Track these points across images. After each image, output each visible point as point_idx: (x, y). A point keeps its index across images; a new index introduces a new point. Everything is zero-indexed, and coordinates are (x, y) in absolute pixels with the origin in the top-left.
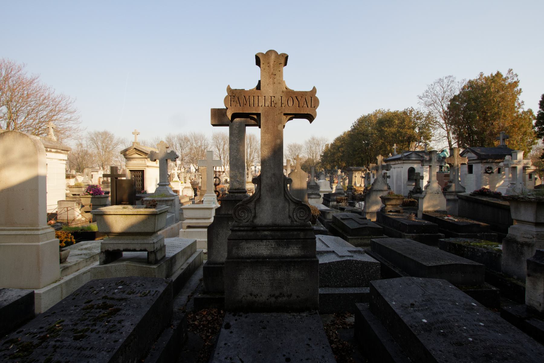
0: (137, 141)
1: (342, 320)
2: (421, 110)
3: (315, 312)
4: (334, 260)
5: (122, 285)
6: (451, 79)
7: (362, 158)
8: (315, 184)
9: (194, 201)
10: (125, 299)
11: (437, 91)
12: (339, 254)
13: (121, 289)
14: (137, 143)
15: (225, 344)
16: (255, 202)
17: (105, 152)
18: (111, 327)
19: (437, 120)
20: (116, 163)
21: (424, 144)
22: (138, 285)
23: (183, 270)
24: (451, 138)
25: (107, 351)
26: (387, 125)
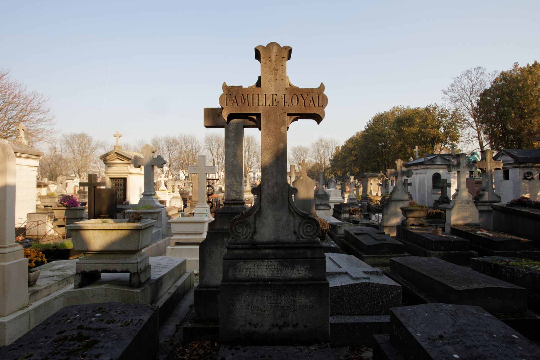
0: (119, 144)
1: (357, 355)
2: (447, 106)
3: (325, 345)
4: (348, 283)
5: (101, 313)
6: (481, 71)
7: (379, 163)
8: (324, 193)
9: (184, 213)
10: (103, 329)
12: (353, 276)
13: (99, 317)
14: (119, 147)
17: (82, 157)
19: (465, 117)
22: (119, 312)
24: (483, 139)
26: (407, 124)
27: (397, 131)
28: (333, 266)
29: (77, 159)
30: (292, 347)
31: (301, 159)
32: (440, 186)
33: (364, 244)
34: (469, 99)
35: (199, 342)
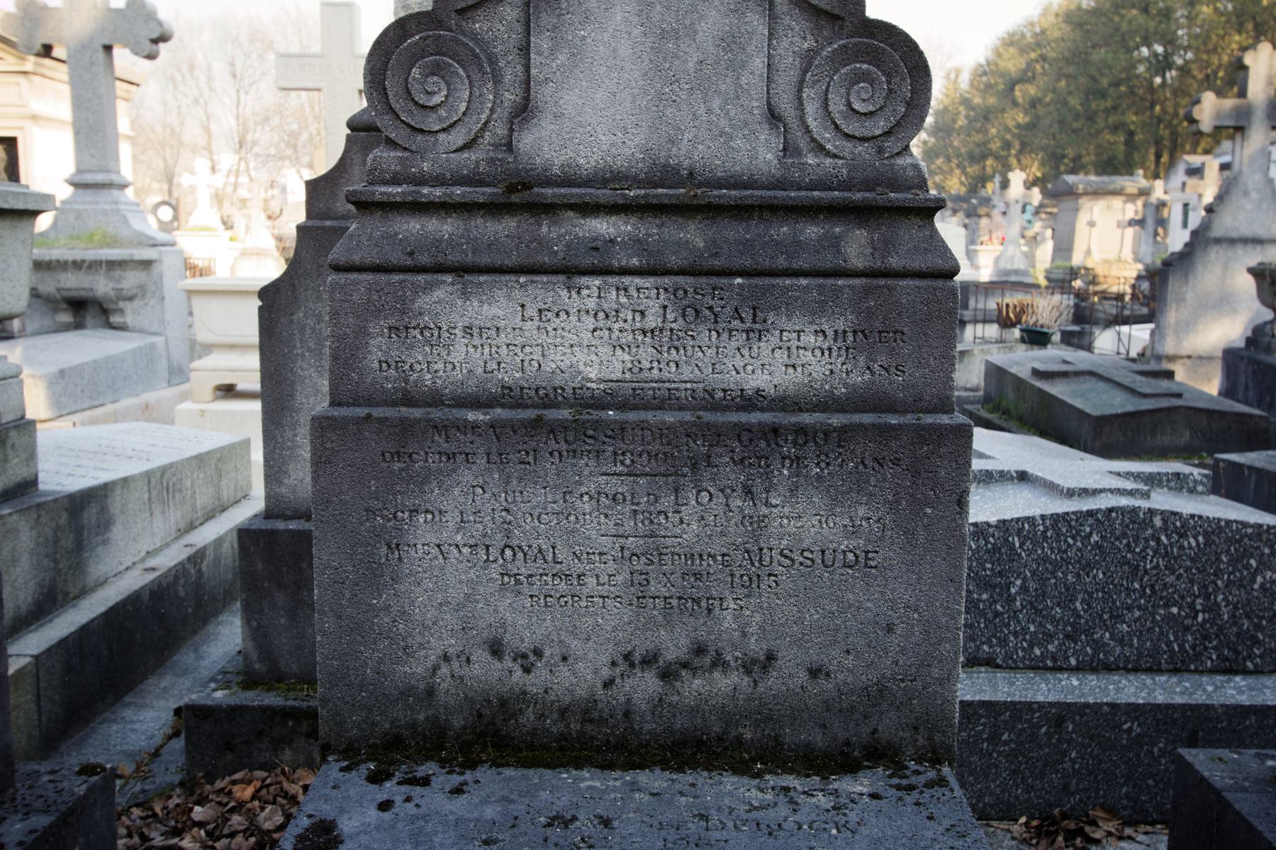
3: (932, 774)
30: (735, 779)
35: (266, 774)
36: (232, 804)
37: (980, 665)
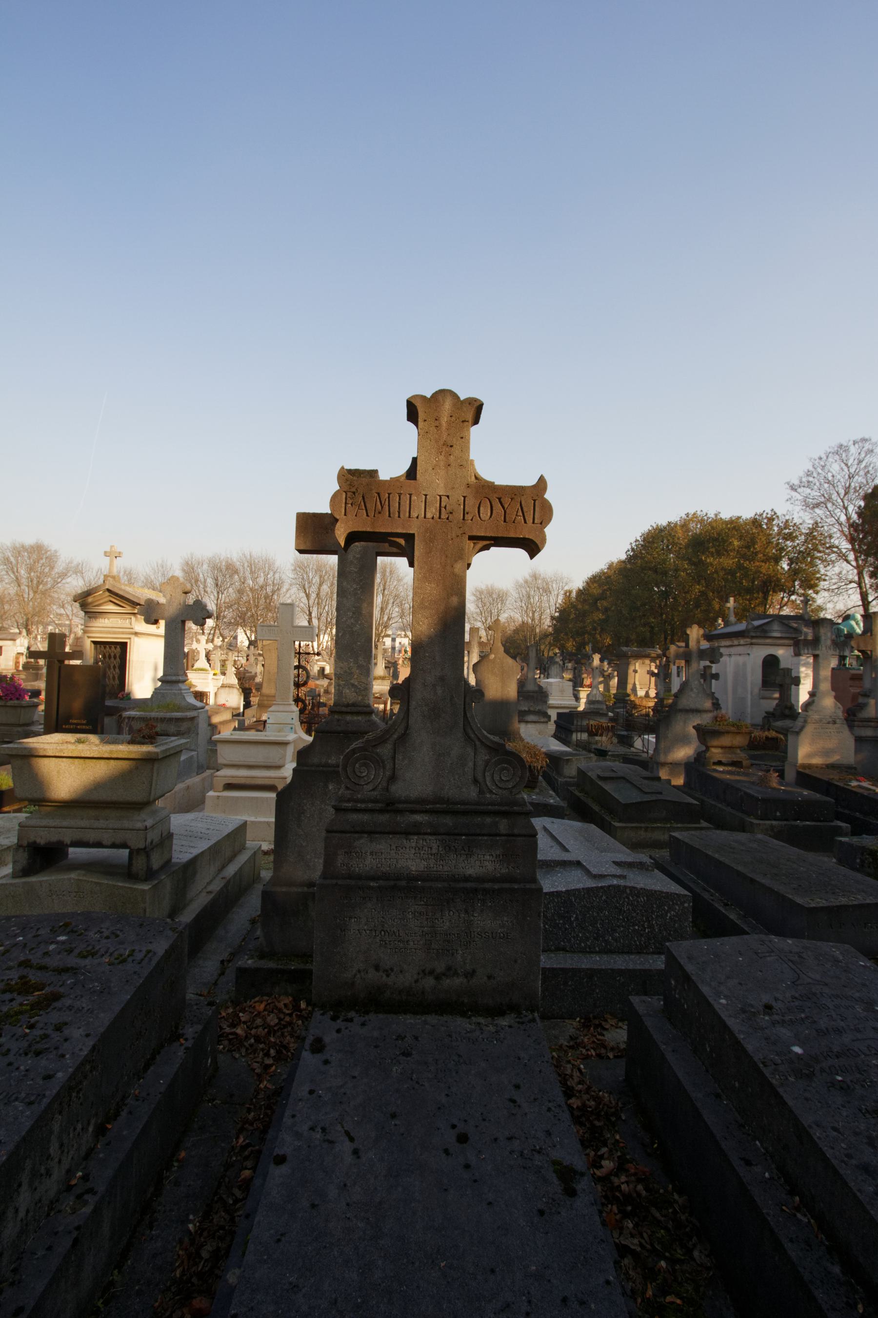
0: (115, 572)
1: (595, 1036)
2: (796, 516)
3: (530, 1017)
4: (580, 886)
5: (67, 934)
6: (867, 446)
7: (652, 628)
8: (537, 689)
9: (244, 721)
10: (72, 968)
11: (834, 473)
12: (591, 869)
13: (63, 942)
14: (114, 577)
15: (311, 1092)
16: (395, 744)
17: (35, 592)
18: (38, 1039)
19: (832, 541)
20: (59, 620)
21: (802, 598)
22: (105, 935)
23: (213, 895)
24: (868, 586)
25: (27, 1100)
26: (713, 550)
27: (692, 565)
28: (552, 847)
29: (24, 598)
31: (491, 614)
32: (777, 682)
33: (617, 800)
34: (842, 504)
36: (255, 1013)
37: (560, 950)
